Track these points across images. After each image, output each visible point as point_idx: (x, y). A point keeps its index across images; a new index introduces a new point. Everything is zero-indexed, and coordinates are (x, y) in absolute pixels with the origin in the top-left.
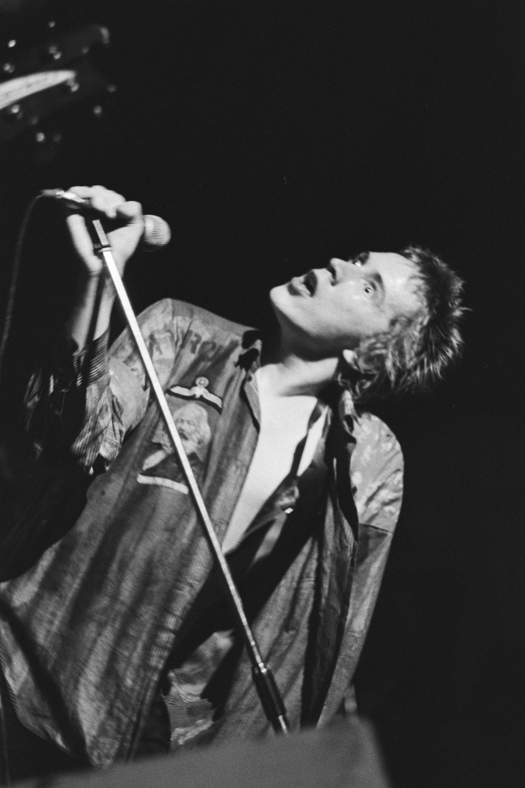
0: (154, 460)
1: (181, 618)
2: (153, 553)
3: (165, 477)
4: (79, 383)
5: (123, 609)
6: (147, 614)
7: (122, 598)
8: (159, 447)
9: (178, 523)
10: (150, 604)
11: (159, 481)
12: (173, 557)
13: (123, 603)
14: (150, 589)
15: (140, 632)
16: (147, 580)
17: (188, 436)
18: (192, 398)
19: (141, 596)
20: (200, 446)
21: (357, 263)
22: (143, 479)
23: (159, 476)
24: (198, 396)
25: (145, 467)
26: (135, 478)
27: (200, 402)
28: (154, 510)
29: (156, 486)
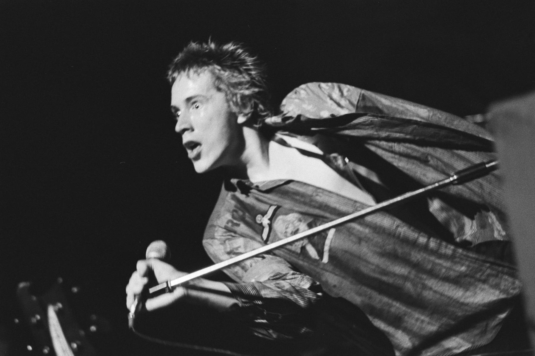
2: (375, 253)
3: (324, 244)
4: (260, 303)
5: (413, 272)
7: (406, 273)
8: (303, 248)
9: (355, 235)
10: (410, 254)
11: (326, 248)
13: (409, 273)
15: (429, 261)
16: (394, 256)
18: (270, 226)
19: (405, 261)
20: (303, 221)
22: (326, 259)
23: (323, 248)
24: (269, 222)
27: (273, 221)
28: (346, 252)
29: (330, 250)
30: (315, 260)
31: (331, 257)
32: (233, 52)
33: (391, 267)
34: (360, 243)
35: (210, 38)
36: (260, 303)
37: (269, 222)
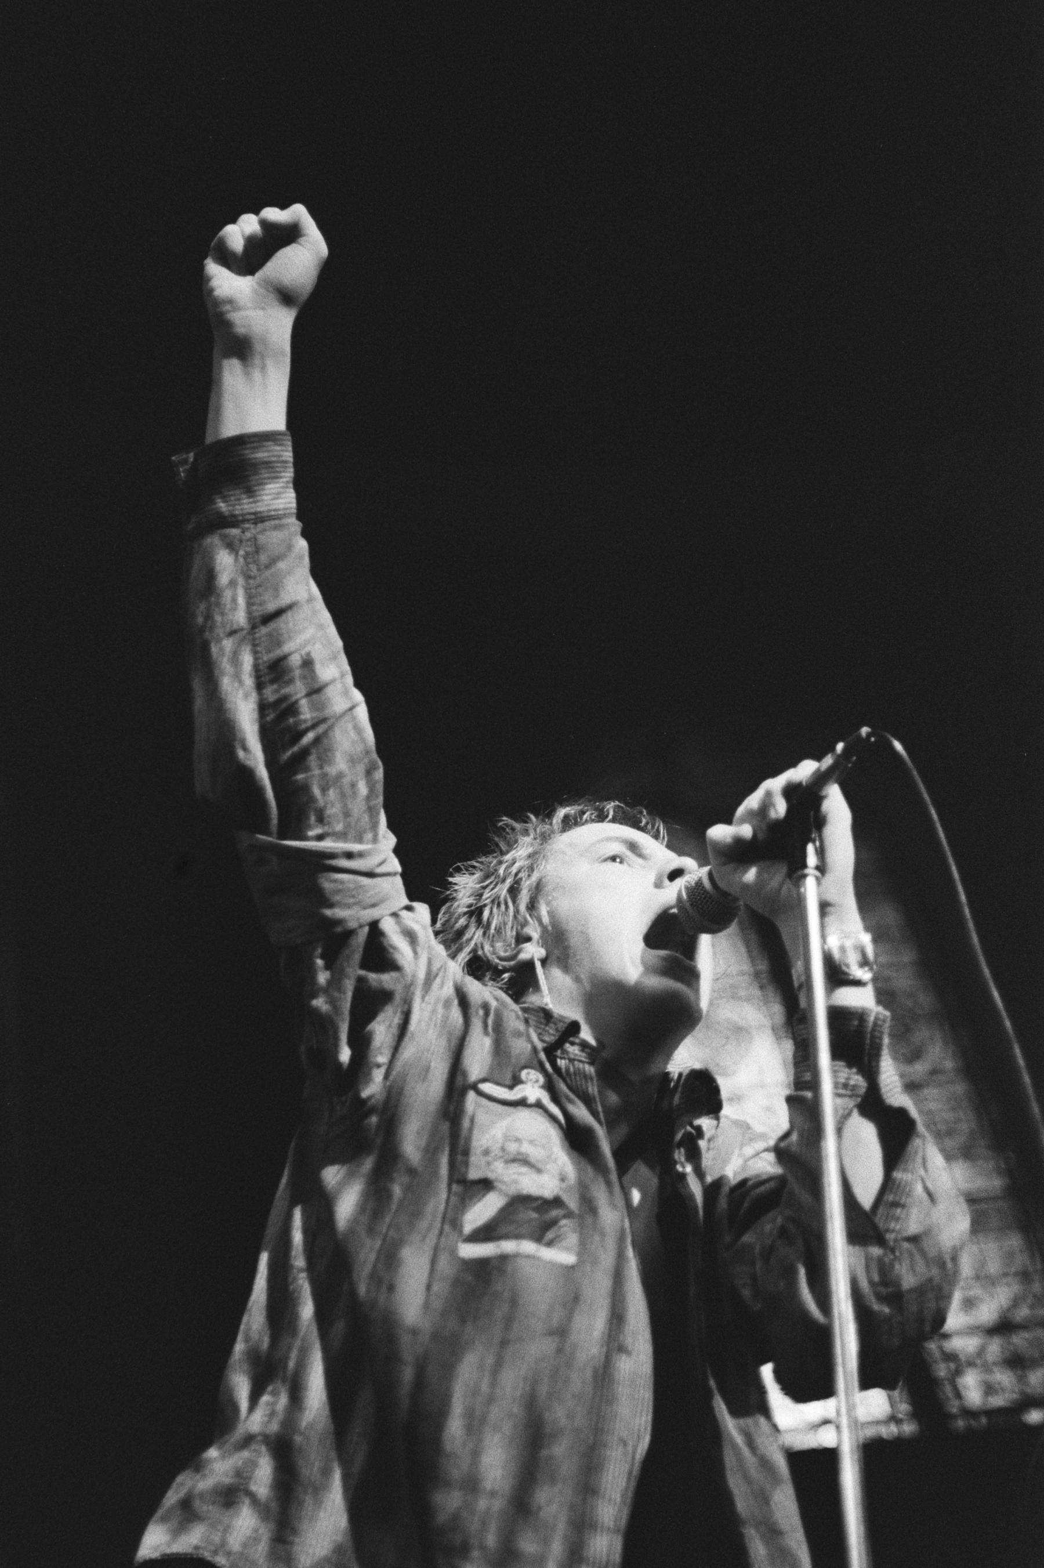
0: (482, 1211)
1: (617, 1531)
2: (534, 1382)
3: (518, 1237)
4: (345, 1055)
5: (498, 1505)
6: (552, 1501)
7: (488, 1485)
8: (486, 1185)
9: (569, 1318)
10: (553, 1481)
11: (508, 1246)
12: (579, 1381)
13: (493, 1494)
14: (544, 1453)
15: (546, 1541)
16: (534, 1437)
17: (540, 1166)
18: (522, 1103)
19: (530, 1470)
20: (564, 1185)
21: (771, 1157)
22: (470, 1251)
23: (506, 1237)
24: (532, 1100)
25: (468, 1228)
26: (453, 1252)
27: (537, 1109)
28: (514, 1302)
29: (504, 1258)
30: (456, 1223)
31: (482, 1268)
32: (833, 749)
33: (497, 1438)
34: (551, 1333)
35: (720, 1406)
36: (345, 1055)
37: (532, 1100)
